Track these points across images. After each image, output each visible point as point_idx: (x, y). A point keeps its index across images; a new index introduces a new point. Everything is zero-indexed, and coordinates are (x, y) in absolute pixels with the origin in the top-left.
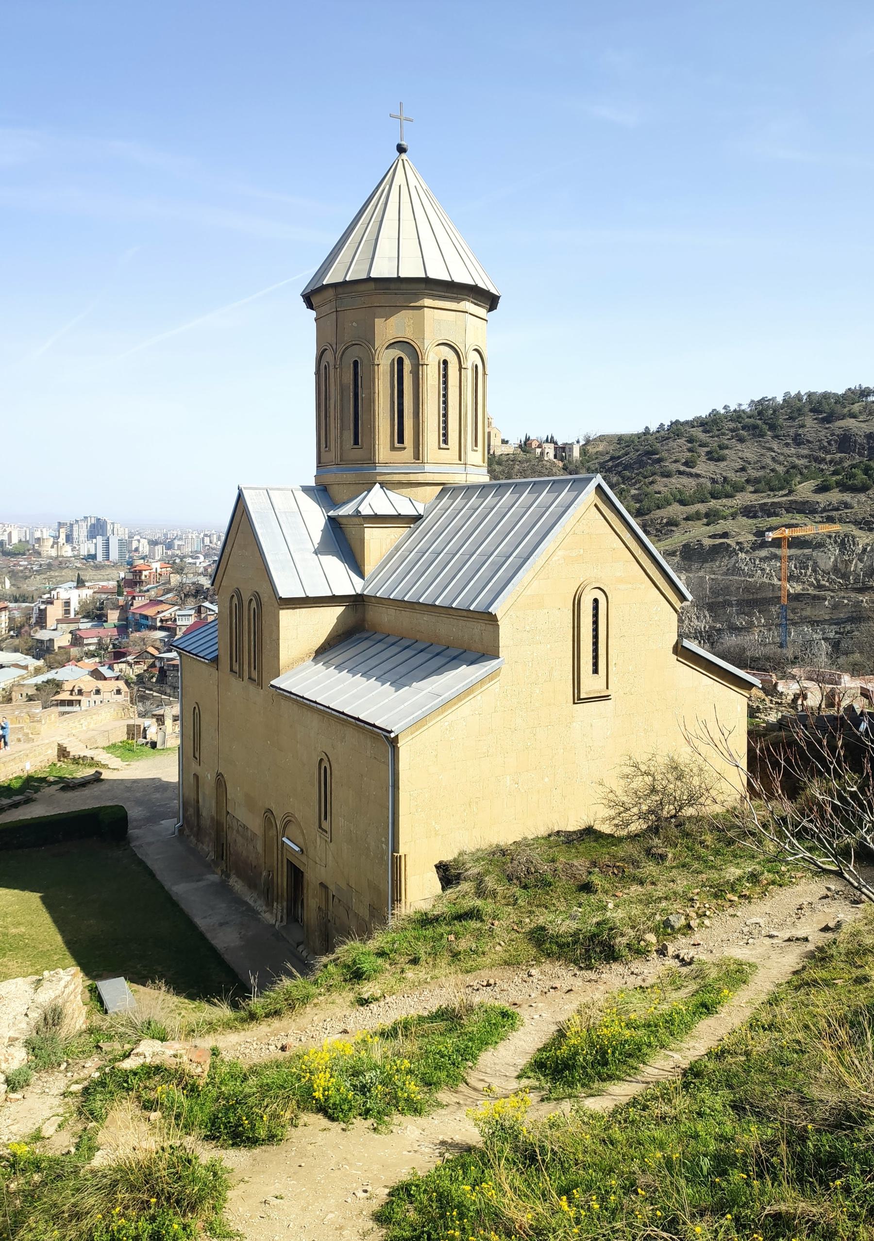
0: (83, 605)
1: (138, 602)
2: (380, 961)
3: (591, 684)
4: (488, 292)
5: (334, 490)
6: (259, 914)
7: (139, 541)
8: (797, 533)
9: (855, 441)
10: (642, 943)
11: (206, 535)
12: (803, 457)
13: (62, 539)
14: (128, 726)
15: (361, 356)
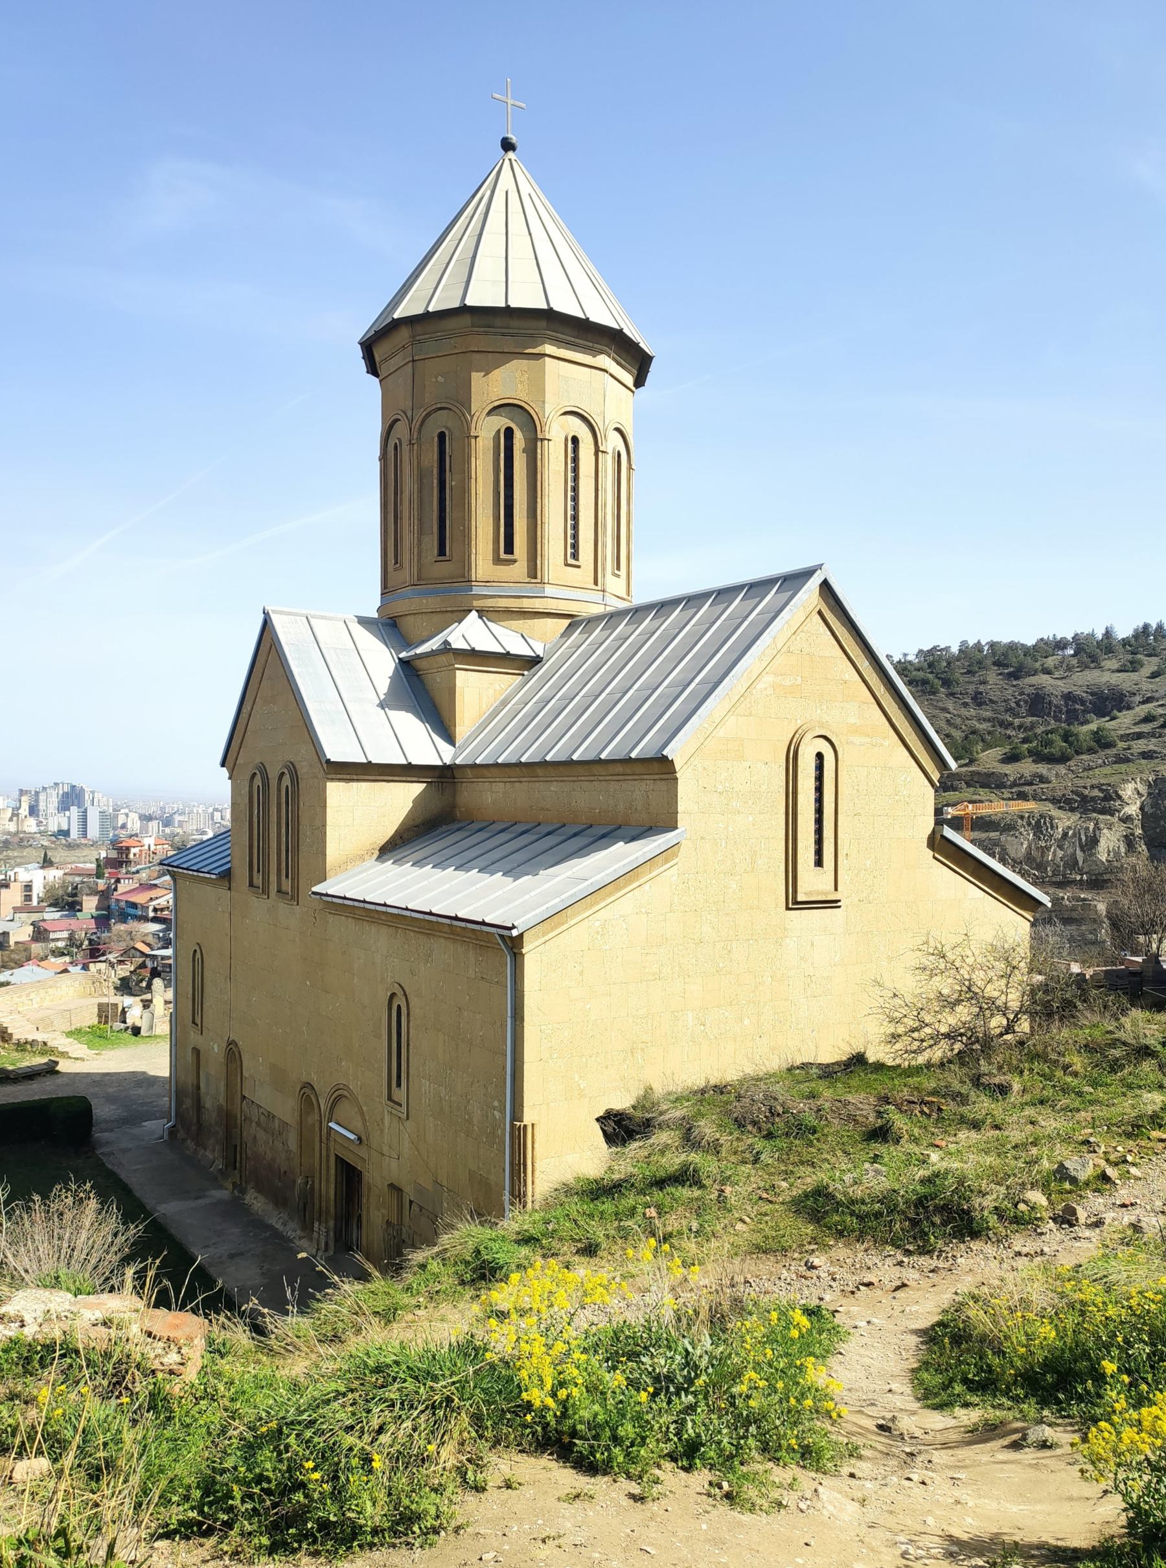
0: (49, 889)
1: (123, 887)
2: (524, 1251)
3: (813, 883)
4: (637, 345)
5: (408, 624)
6: (292, 1241)
7: (127, 815)
8: (984, 810)
9: (1050, 702)
10: (1022, 1206)
11: (216, 810)
12: (985, 720)
13: (24, 811)
14: (100, 1005)
15: (449, 425)
